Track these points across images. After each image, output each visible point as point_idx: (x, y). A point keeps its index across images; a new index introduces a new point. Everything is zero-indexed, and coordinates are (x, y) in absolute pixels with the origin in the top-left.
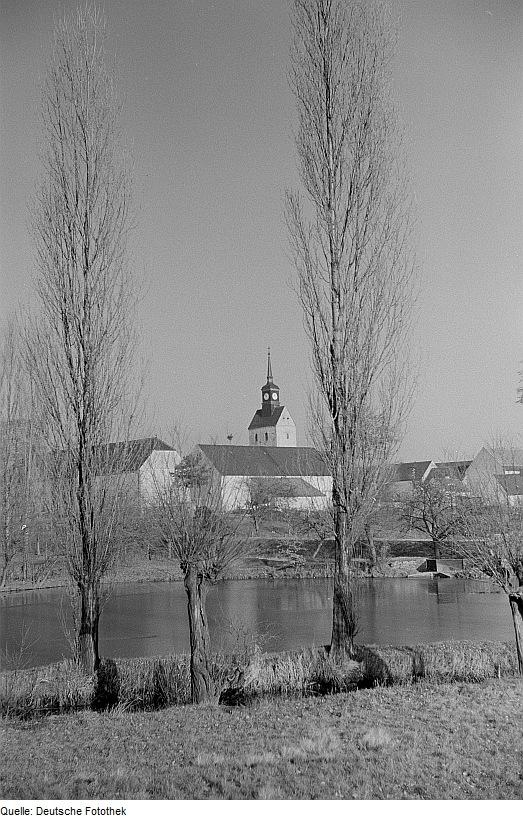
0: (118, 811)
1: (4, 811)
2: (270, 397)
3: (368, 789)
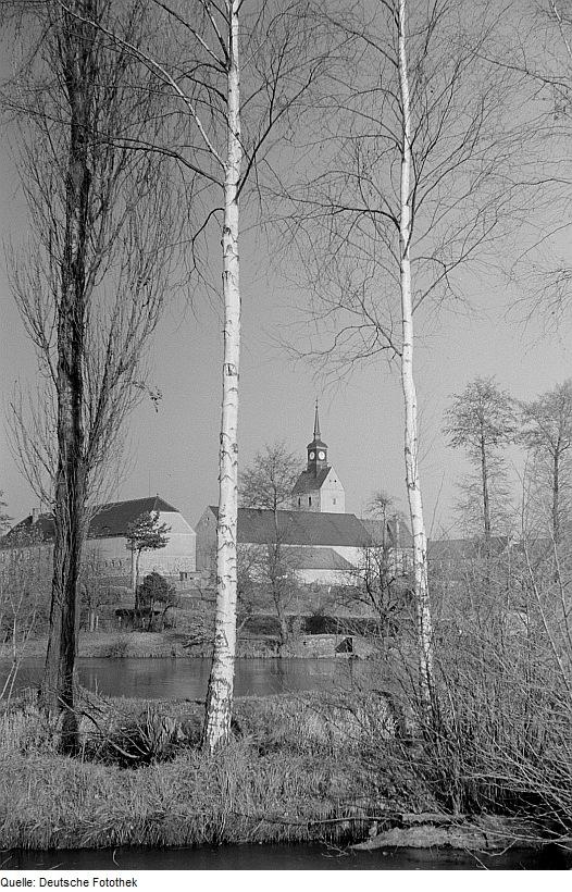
1: (4, 882)
2: (316, 456)
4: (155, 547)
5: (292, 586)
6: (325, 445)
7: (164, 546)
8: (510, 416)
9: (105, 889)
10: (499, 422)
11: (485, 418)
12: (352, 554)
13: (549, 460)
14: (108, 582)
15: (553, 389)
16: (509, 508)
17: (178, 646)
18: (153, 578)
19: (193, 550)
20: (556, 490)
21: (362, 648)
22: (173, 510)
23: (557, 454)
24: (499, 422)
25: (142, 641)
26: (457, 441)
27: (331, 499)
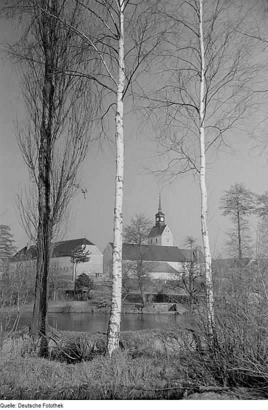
0: (59, 405)
1: (2, 405)
2: (160, 220)
4: (84, 261)
5: (148, 280)
7: (88, 261)
8: (252, 201)
11: (240, 202)
12: (176, 265)
14: (62, 277)
16: (250, 244)
17: (94, 307)
18: (83, 276)
19: (101, 263)
21: (181, 309)
22: (93, 244)
25: (77, 305)
26: (225, 213)
27: (167, 239)
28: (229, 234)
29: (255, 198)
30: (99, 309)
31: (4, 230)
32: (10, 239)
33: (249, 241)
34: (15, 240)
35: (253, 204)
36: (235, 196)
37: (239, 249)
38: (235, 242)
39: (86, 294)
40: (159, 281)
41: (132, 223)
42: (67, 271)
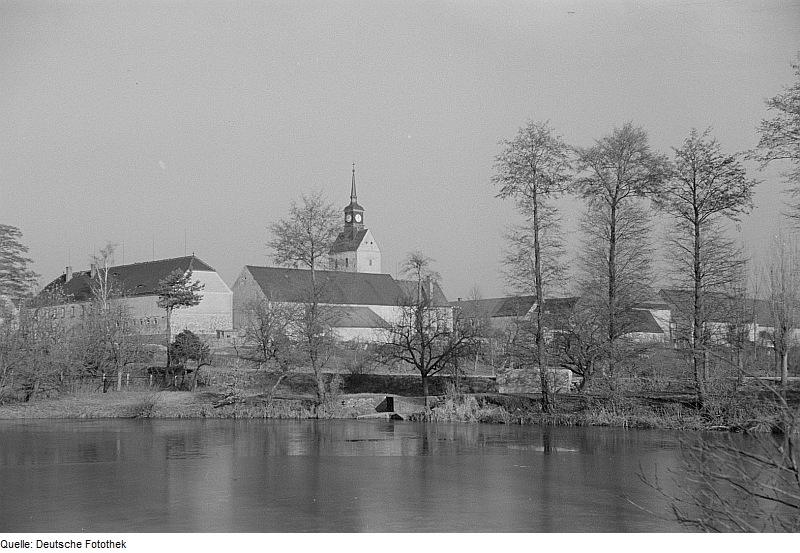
0: (118, 544)
1: (4, 544)
2: (353, 218)
3: (218, 472)
4: (188, 304)
5: (329, 344)
6: (362, 209)
7: (197, 304)
8: (565, 164)
9: (97, 550)
10: (552, 170)
11: (538, 166)
12: (390, 313)
13: (606, 210)
14: (137, 339)
15: (611, 133)
16: (562, 260)
17: (208, 406)
18: (186, 336)
19: (229, 309)
20: (613, 240)
21: (404, 407)
22: (209, 269)
23: (615, 202)
24: (552, 170)
25: (170, 400)
26: (505, 192)
27: (367, 259)
28: (513, 239)
29: (572, 156)
30: (218, 410)
31: (7, 235)
32: (22, 255)
33: (558, 254)
34: (33, 259)
35: (568, 168)
36: (527, 152)
37: (537, 273)
38: (526, 257)
39: (192, 374)
40: (353, 345)
41: (293, 216)
42: (155, 326)
